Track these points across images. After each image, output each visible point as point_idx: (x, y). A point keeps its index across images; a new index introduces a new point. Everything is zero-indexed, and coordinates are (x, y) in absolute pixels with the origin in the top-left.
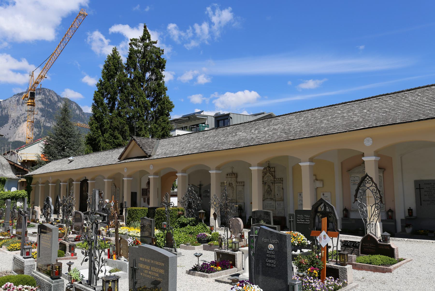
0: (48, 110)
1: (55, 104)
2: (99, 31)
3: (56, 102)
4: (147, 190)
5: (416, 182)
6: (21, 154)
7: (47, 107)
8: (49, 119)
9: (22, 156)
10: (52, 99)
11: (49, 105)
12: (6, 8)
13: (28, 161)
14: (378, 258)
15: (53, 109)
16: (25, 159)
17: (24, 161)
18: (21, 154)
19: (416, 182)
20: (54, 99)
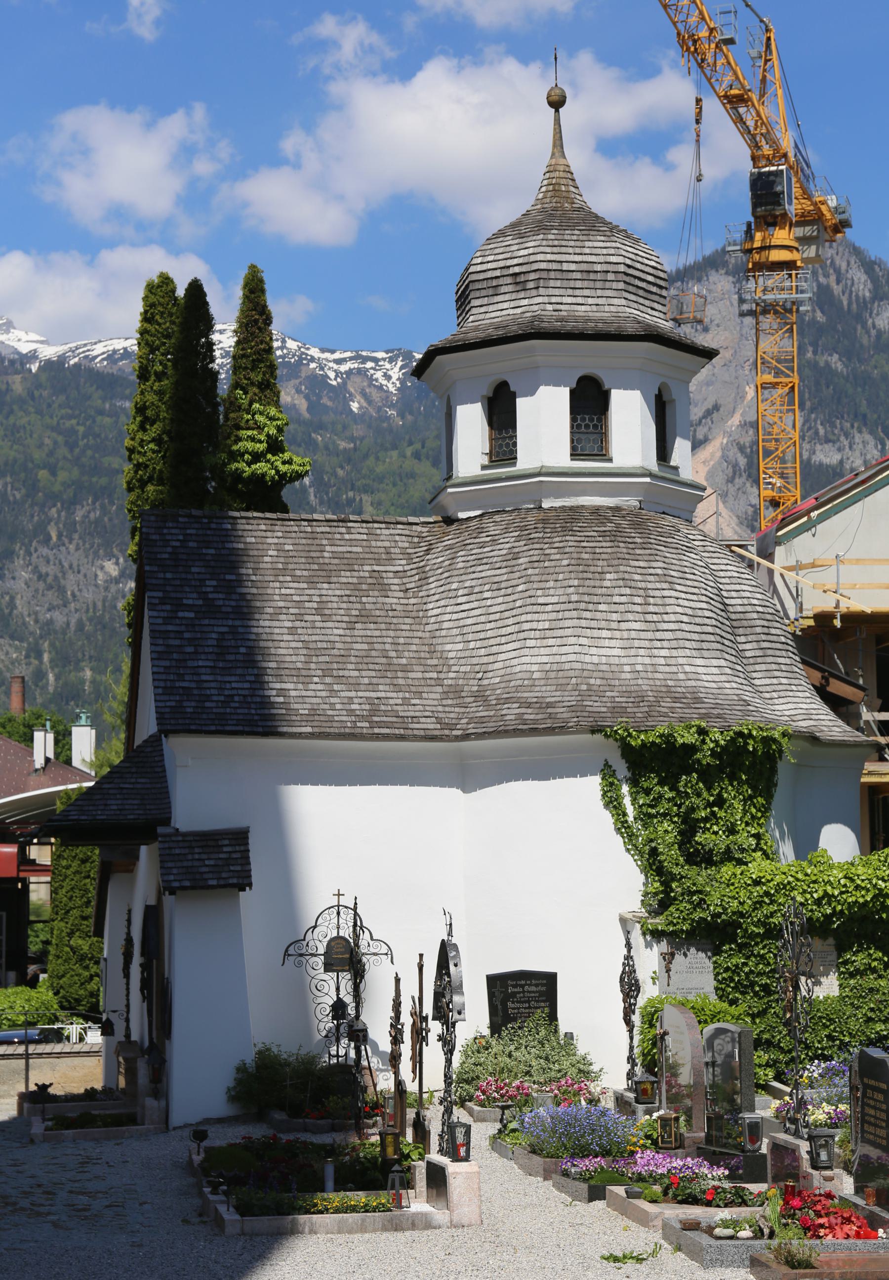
0: (822, 360)
1: (859, 318)
2: (547, 384)
3: (864, 305)
4: (173, 722)
5: (549, 981)
6: (797, 568)
7: (815, 344)
8: (829, 422)
9: (806, 580)
10: (837, 289)
11: (821, 330)
12: (460, 69)
13: (854, 619)
14: (452, 954)
15: (848, 355)
16: (826, 604)
17: (823, 619)
18: (797, 568)
19: (549, 981)
20: (848, 290)
